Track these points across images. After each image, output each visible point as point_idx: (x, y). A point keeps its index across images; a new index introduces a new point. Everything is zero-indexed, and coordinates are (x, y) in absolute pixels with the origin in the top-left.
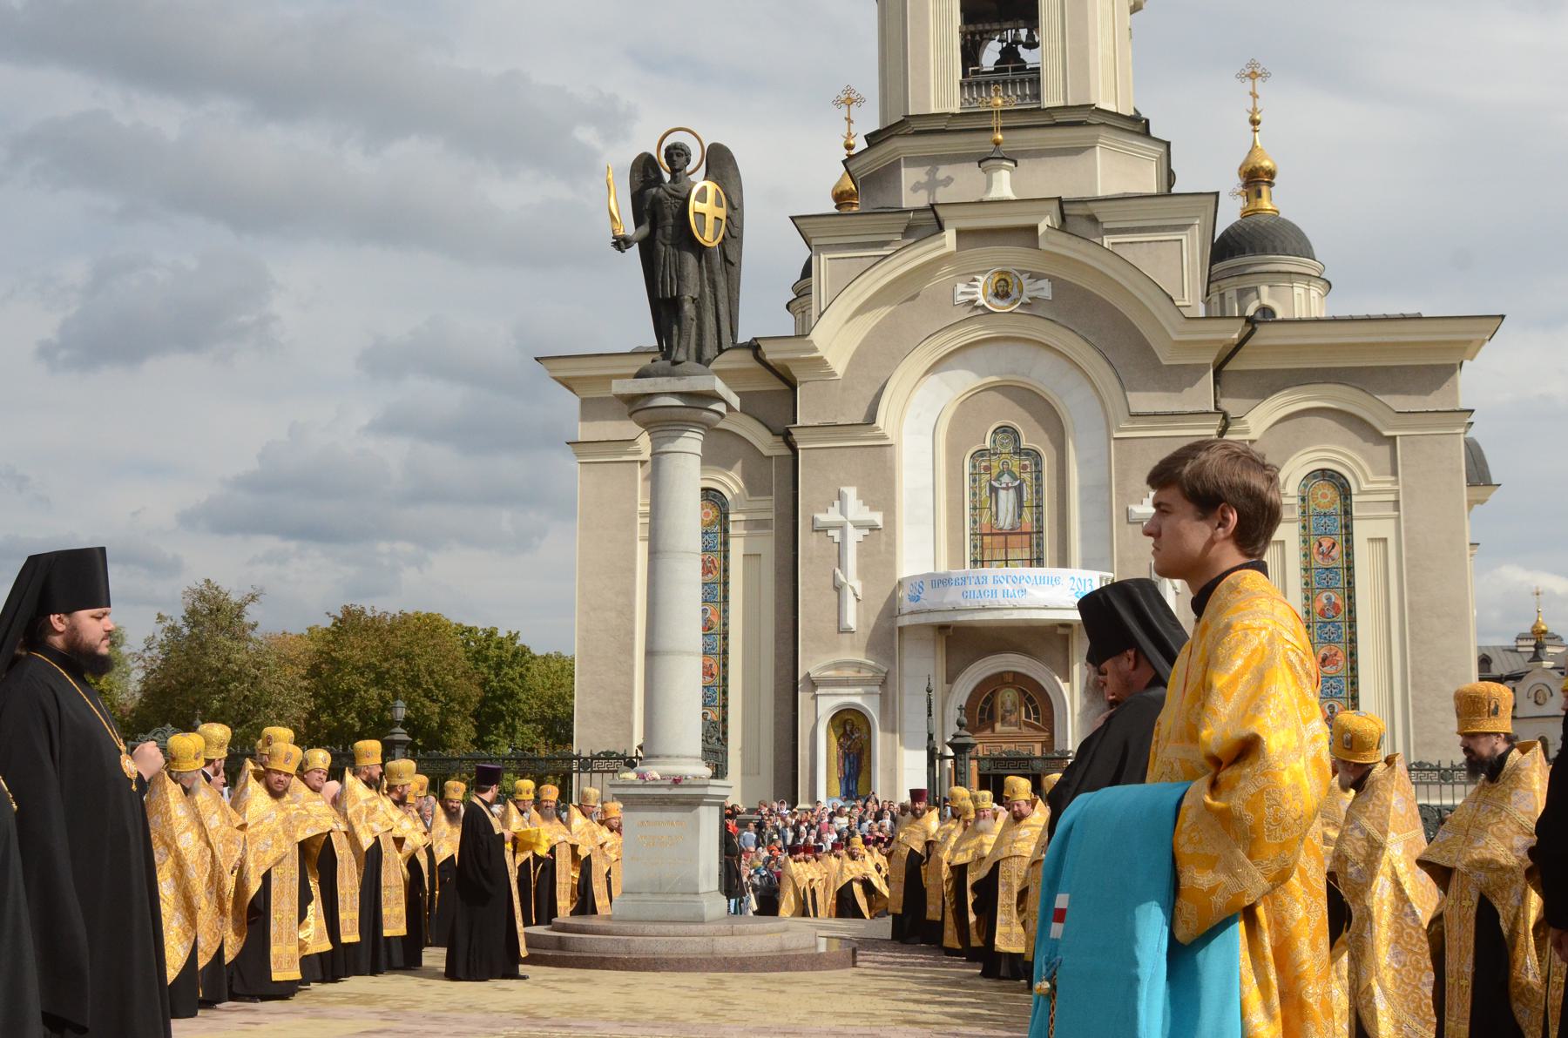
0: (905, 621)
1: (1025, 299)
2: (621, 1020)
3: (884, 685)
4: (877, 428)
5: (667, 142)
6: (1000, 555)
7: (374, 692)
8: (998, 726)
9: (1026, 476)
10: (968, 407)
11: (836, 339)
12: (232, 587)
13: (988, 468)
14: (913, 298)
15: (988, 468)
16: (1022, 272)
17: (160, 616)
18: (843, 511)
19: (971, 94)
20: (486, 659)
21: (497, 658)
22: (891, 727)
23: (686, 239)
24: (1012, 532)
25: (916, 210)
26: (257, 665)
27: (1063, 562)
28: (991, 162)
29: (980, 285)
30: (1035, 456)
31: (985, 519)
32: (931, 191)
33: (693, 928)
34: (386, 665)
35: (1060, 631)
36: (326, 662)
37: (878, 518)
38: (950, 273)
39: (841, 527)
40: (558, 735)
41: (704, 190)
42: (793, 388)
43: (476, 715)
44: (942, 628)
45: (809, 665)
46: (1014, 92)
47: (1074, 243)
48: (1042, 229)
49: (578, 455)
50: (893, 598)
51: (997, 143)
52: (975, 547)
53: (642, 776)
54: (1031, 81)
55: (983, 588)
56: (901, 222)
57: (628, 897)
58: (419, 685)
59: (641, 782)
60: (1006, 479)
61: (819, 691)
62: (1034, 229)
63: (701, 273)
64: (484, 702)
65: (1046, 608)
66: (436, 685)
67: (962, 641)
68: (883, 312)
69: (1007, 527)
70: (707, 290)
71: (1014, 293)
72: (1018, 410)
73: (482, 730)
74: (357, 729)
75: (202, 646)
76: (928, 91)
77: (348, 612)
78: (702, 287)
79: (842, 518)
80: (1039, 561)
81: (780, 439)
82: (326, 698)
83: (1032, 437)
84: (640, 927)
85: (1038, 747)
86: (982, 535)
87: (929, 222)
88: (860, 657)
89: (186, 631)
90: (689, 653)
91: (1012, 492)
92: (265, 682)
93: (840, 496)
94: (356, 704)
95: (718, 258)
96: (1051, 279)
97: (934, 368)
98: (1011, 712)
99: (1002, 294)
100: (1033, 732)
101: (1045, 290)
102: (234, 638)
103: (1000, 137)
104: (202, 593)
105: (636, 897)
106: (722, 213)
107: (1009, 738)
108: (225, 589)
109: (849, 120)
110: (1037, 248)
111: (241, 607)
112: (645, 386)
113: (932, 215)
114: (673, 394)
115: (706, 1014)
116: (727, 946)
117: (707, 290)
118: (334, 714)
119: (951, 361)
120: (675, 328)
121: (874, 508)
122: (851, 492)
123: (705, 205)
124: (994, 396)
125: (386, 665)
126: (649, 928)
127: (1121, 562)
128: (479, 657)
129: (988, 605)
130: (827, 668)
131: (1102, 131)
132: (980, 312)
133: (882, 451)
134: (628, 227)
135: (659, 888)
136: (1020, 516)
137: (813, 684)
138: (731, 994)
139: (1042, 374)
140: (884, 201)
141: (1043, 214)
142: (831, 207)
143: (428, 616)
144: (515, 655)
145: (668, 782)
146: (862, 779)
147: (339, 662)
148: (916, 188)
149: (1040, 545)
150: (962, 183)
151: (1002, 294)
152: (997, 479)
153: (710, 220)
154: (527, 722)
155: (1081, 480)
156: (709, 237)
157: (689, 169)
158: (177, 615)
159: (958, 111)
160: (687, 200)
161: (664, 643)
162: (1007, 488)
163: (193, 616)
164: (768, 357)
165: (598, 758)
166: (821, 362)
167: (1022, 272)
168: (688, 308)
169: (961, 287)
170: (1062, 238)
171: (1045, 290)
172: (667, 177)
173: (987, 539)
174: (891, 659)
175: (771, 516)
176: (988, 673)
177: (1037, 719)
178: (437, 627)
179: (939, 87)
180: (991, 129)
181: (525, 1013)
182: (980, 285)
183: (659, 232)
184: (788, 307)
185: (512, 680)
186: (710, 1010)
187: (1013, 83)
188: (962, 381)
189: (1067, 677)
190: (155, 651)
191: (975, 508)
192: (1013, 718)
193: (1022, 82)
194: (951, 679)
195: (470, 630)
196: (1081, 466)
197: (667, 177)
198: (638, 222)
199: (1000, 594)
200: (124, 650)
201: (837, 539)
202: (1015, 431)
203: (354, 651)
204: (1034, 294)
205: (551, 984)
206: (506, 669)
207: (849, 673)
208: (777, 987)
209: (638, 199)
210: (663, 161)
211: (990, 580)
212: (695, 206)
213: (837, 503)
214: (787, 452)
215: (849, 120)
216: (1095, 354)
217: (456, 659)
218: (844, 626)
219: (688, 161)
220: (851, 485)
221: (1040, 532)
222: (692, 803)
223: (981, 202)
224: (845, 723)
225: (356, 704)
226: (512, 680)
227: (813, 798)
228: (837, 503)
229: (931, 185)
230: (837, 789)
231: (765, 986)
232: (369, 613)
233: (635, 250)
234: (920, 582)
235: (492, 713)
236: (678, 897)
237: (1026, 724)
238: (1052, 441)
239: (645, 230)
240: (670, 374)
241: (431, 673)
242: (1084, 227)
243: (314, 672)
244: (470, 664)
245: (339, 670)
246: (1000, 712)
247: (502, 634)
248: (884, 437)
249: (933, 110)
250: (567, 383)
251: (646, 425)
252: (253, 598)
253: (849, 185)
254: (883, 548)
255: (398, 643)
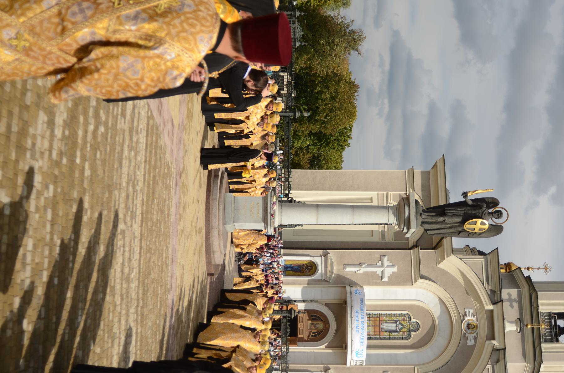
0: (348, 289)
1: (467, 335)
2: (179, 203)
3: (325, 281)
4: (418, 279)
5: (503, 211)
6: (372, 324)
7: (328, 96)
8: (310, 322)
9: (401, 334)
10: (426, 313)
11: (452, 264)
12: (364, 47)
13: (404, 320)
14: (467, 293)
15: (404, 320)
16: (477, 334)
17: (353, 21)
18: (388, 266)
19: (546, 316)
20: (340, 135)
21: (341, 139)
22: (310, 283)
23: (467, 218)
24: (380, 328)
25: (501, 295)
26: (336, 55)
27: (369, 347)
28: (519, 323)
29: (472, 318)
30: (409, 337)
31: (385, 319)
32: (508, 300)
33: (221, 221)
34: (338, 101)
35: (344, 345)
36: (339, 79)
37: (385, 279)
38: (477, 307)
39: (382, 266)
40: (314, 161)
41: (485, 224)
42: (434, 248)
43: (320, 132)
44: (345, 302)
45: (332, 253)
46: (547, 332)
47: (488, 354)
48: (494, 342)
49: (409, 170)
50: (356, 284)
51: (527, 325)
52: (375, 315)
53: (274, 203)
54: (552, 339)
55: (359, 317)
56: (496, 289)
57: (233, 198)
58: (330, 112)
59: (272, 203)
60: (400, 326)
61: (323, 257)
62: (494, 339)
63: (455, 223)
64: (325, 135)
65: (352, 340)
66: (331, 118)
67: (341, 309)
68: (462, 282)
69: (382, 326)
70: (449, 225)
71: (469, 331)
72: (425, 332)
73: (315, 134)
74: (315, 91)
75: (342, 36)
76: (547, 300)
77: (357, 86)
78: (449, 224)
79: (385, 266)
80: (369, 338)
81: (415, 244)
82: (326, 79)
83: (415, 336)
84: (222, 203)
85: (302, 336)
86: (379, 318)
87: (496, 299)
88: (335, 272)
89: (348, 30)
90: (317, 219)
91: (395, 328)
92: (330, 58)
93: (394, 266)
94: (324, 90)
95: (460, 229)
96: (475, 345)
97: (441, 300)
98: (315, 327)
99: (469, 326)
100: (307, 335)
101: (471, 342)
102: (346, 47)
103: (529, 327)
104: (361, 35)
105: (233, 201)
106: (477, 231)
107: (305, 326)
108: (363, 44)
109: (539, 269)
110: (487, 340)
111: (357, 49)
112: (413, 204)
113: (499, 300)
114: (409, 214)
115: (182, 231)
116: (215, 233)
117: (449, 225)
118: (320, 82)
119: (444, 307)
120: (434, 214)
121: (389, 277)
122: (395, 269)
123: (480, 224)
124: (431, 322)
125: (338, 101)
126: (221, 207)
127: (369, 369)
128: (341, 133)
129: (353, 319)
130: (331, 261)
131: (532, 366)
132: (462, 318)
133: (411, 282)
134: (471, 196)
135: (236, 209)
136: (386, 331)
137: (325, 255)
138: (193, 237)
139: (439, 341)
140: (505, 282)
141: (499, 343)
142: (502, 262)
143: (356, 116)
144: (342, 146)
145: (272, 212)
146: (291, 272)
147: (339, 84)
148: (509, 294)
149: (375, 338)
150: (511, 312)
151: (469, 326)
152: (400, 323)
153: (474, 226)
154: (319, 150)
155: (399, 354)
156: (467, 226)
157: (493, 219)
158: (354, 27)
159: (539, 311)
160: (481, 218)
161: (321, 211)
162: (396, 327)
163: (353, 32)
164: (445, 239)
165: (289, 184)
166: (443, 259)
167: (477, 334)
168: (441, 219)
169: (471, 311)
170: (490, 349)
171: (471, 342)
172: (490, 211)
173: (378, 319)
174: (333, 284)
175: (387, 240)
176: (329, 319)
177: (312, 336)
178: (351, 118)
179: (548, 304)
180: (532, 323)
181: (184, 167)
182: (472, 318)
183: (469, 208)
184: (467, 245)
185: (333, 145)
186: (185, 232)
187: (551, 332)
188: (436, 311)
189: (327, 347)
190: (340, 20)
191: (389, 315)
192: (313, 327)
193: (551, 335)
194: (327, 305)
195: (351, 130)
196: (405, 354)
197: (490, 211)
198: (473, 200)
199: (357, 323)
200: (342, 9)
201: (378, 264)
202: (417, 330)
203: (343, 89)
204: (469, 338)
205: (198, 176)
206: (336, 143)
207: (329, 268)
208: (197, 251)
209: (482, 200)
210: (496, 209)
211: (362, 320)
212: (479, 221)
213: (391, 264)
214: (410, 246)
215: (539, 269)
216: (447, 360)
217: (340, 125)
218: (346, 266)
219: (496, 218)
220: (398, 269)
221: (380, 339)
222: (265, 221)
223: (504, 319)
224: (312, 266)
225: (324, 90)
226: (333, 145)
227: (285, 255)
228: (391, 264)
229: (510, 300)
230: (288, 263)
231: (198, 248)
232: (356, 94)
233: (462, 199)
234: (362, 294)
235: (321, 138)
236: (233, 216)
237: (310, 332)
238: (414, 344)
239: (470, 203)
240: (417, 212)
241: (335, 116)
242: (495, 357)
243: (336, 75)
244: (338, 130)
245: (336, 83)
246: (315, 322)
247: (349, 141)
248: (415, 282)
249: (539, 301)
250: (435, 166)
251: (399, 204)
252: (360, 54)
253: (513, 268)
254: (375, 281)
255: (346, 105)
